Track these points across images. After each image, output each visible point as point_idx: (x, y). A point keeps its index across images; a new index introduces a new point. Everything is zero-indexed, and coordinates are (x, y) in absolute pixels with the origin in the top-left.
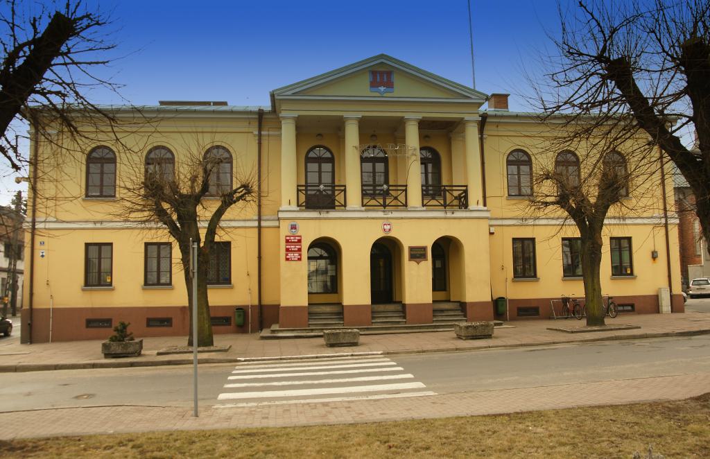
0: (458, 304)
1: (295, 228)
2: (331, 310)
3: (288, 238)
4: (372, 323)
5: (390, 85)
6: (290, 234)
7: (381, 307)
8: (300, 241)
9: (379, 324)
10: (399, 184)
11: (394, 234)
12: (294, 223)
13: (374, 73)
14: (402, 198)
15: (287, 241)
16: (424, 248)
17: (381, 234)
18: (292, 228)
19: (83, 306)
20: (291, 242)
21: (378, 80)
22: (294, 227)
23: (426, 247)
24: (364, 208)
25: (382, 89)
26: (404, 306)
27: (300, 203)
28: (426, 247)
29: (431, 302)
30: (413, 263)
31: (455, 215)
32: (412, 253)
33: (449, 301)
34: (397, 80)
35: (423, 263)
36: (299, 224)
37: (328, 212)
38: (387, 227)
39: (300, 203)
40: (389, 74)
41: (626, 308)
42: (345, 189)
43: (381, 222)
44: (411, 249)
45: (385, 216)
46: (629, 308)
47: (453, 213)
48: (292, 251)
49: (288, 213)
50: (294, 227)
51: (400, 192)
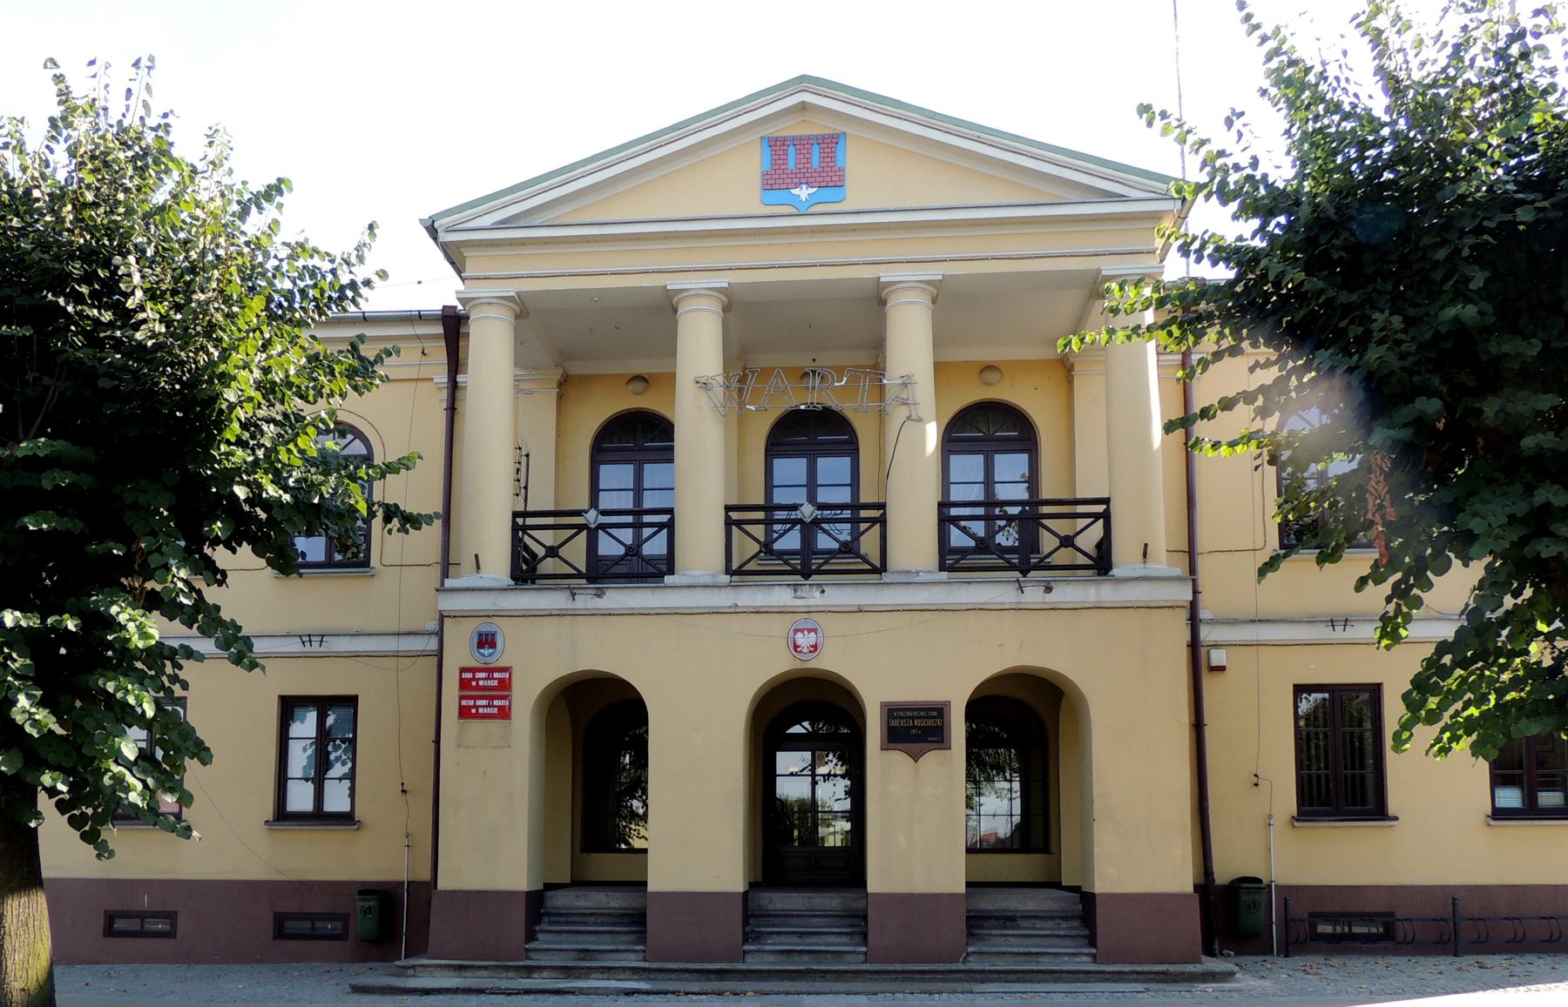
0: (1076, 896)
1: (493, 645)
2: (625, 904)
3: (466, 675)
4: (745, 952)
5: (830, 178)
6: (473, 664)
7: (779, 900)
8: (505, 685)
9: (1010, 959)
10: (1080, 495)
11: (831, 661)
12: (485, 629)
13: (777, 145)
14: (869, 543)
15: (464, 684)
16: (938, 712)
17: (779, 664)
18: (481, 645)
19: (85, 876)
20: (478, 688)
21: (792, 164)
22: (486, 641)
23: (948, 704)
24: (945, 575)
25: (803, 192)
26: (1088, 900)
27: (735, 566)
28: (948, 704)
29: (962, 889)
30: (899, 759)
31: (1052, 597)
32: (895, 723)
33: (1057, 885)
34: (855, 160)
35: (932, 759)
36: (506, 632)
37: (600, 594)
38: (804, 640)
39: (735, 566)
40: (830, 143)
41: (134, 925)
42: (672, 520)
43: (781, 626)
44: (892, 712)
45: (799, 602)
46: (119, 925)
47: (1048, 589)
48: (478, 716)
49: (468, 595)
50: (486, 641)
51: (1082, 523)
